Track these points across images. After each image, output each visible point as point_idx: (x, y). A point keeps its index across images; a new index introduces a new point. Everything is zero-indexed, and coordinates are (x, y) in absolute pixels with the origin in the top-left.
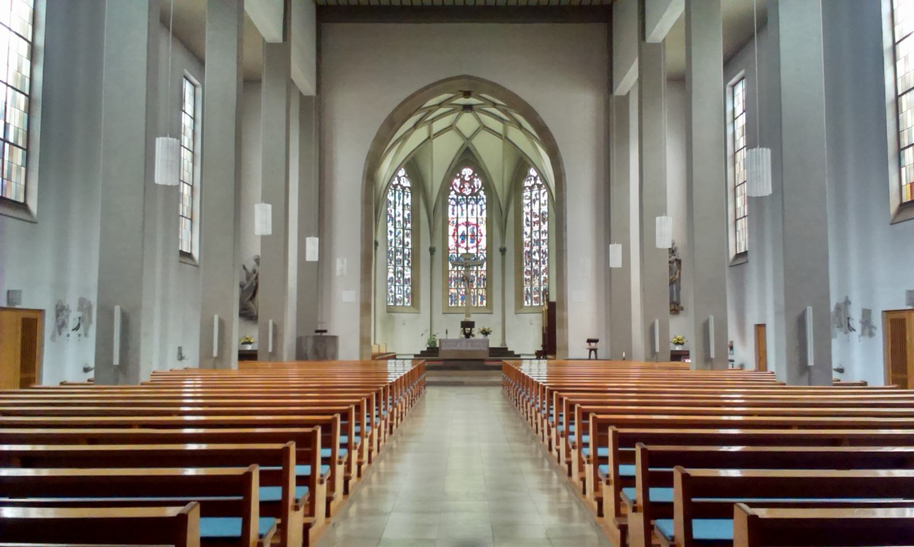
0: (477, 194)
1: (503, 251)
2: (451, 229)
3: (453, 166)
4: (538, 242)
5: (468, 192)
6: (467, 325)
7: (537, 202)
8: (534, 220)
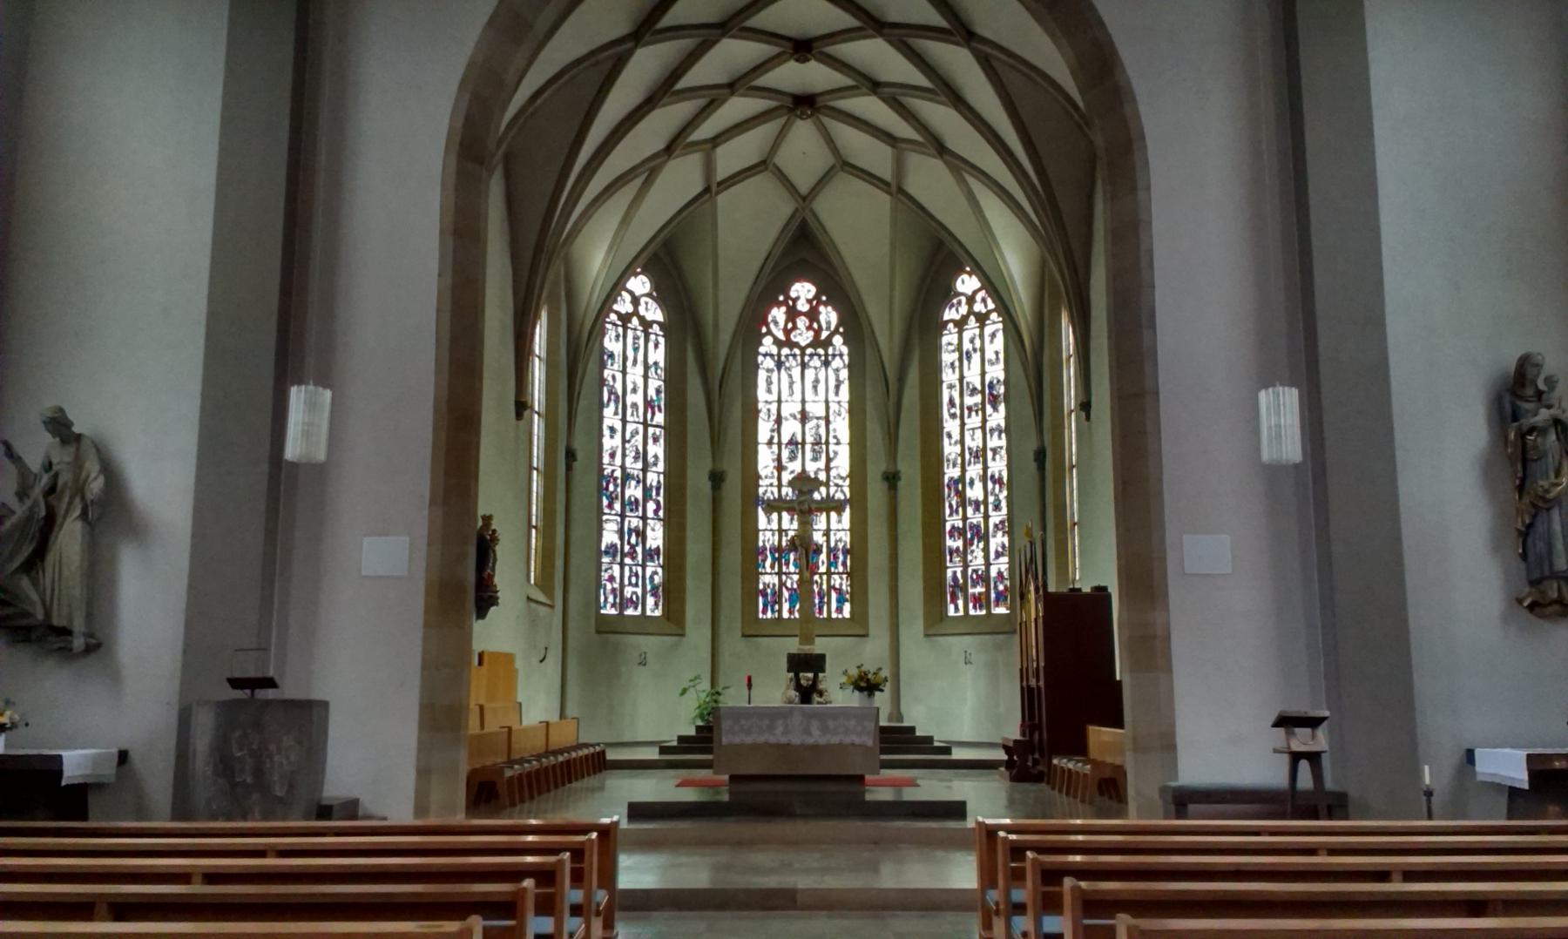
0: (828, 343)
1: (892, 479)
2: (764, 429)
3: (763, 283)
4: (980, 454)
5: (803, 337)
6: (806, 665)
7: (976, 357)
8: (969, 401)
